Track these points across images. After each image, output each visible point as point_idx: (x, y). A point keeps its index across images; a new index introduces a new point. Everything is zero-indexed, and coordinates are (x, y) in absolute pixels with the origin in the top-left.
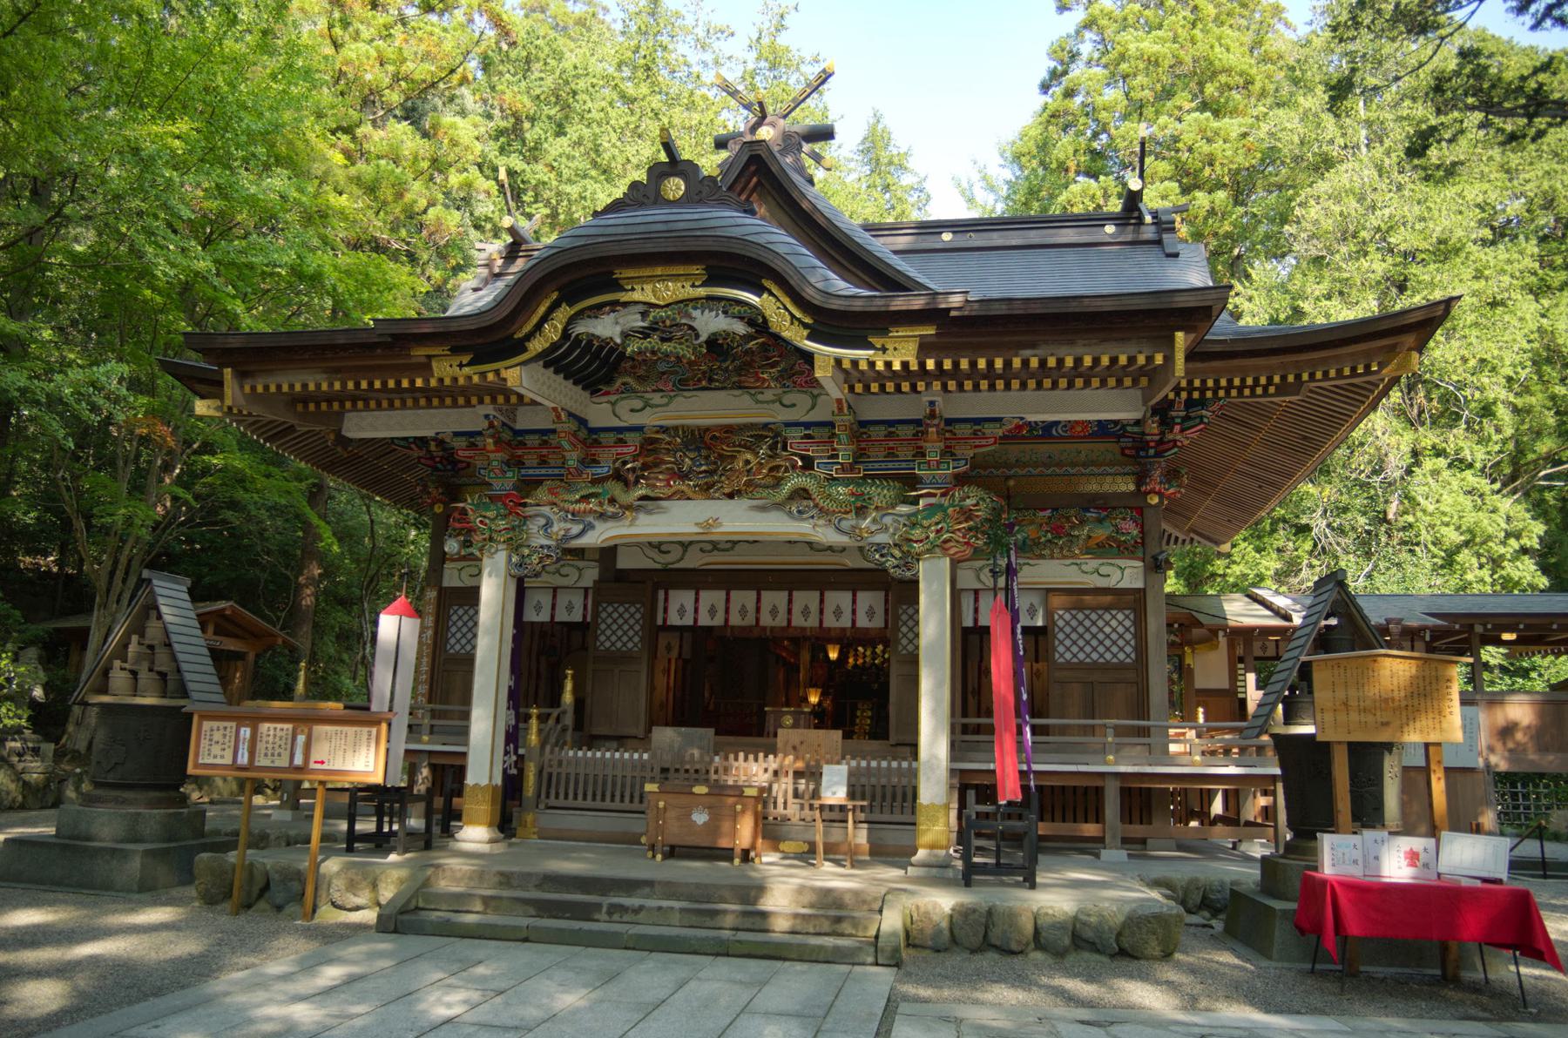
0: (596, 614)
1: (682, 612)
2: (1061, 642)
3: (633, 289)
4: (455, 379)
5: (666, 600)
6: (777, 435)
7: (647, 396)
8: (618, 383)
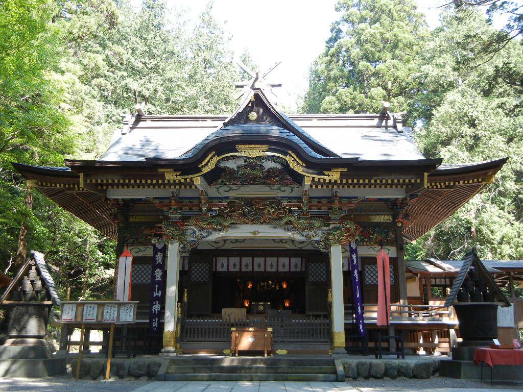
0: (190, 267)
1: (222, 266)
2: (367, 277)
3: (241, 151)
4: (174, 181)
5: (216, 261)
6: (279, 201)
7: (231, 186)
8: (220, 181)
